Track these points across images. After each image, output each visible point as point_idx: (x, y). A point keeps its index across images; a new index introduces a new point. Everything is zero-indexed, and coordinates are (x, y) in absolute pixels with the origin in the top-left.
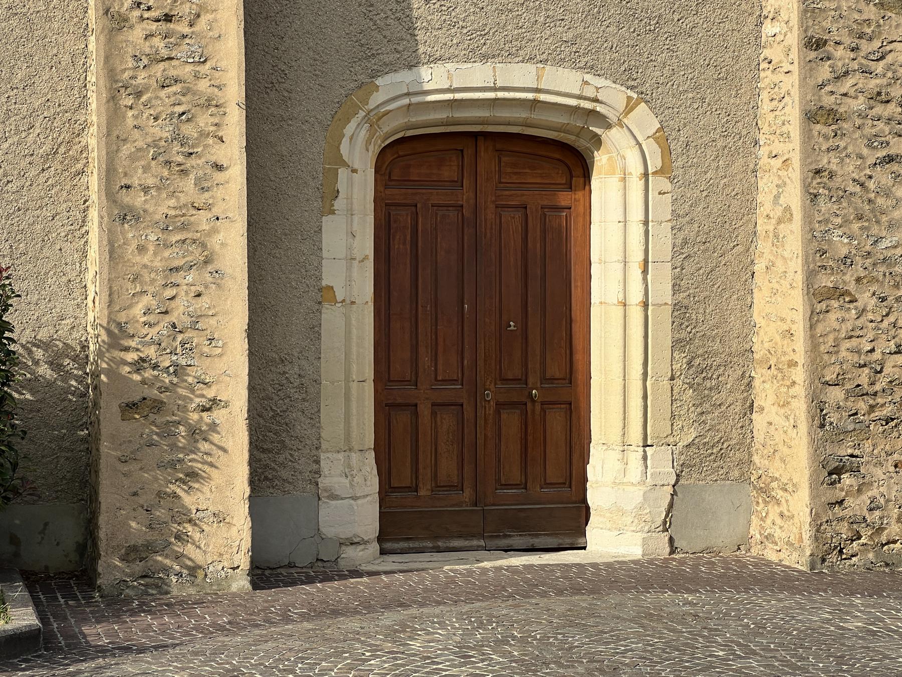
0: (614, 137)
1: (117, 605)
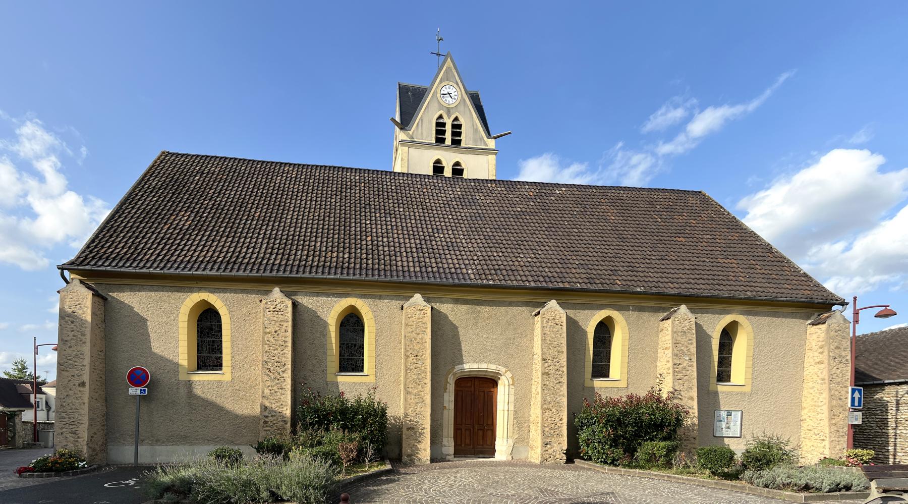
0: (502, 378)
1: (406, 465)
